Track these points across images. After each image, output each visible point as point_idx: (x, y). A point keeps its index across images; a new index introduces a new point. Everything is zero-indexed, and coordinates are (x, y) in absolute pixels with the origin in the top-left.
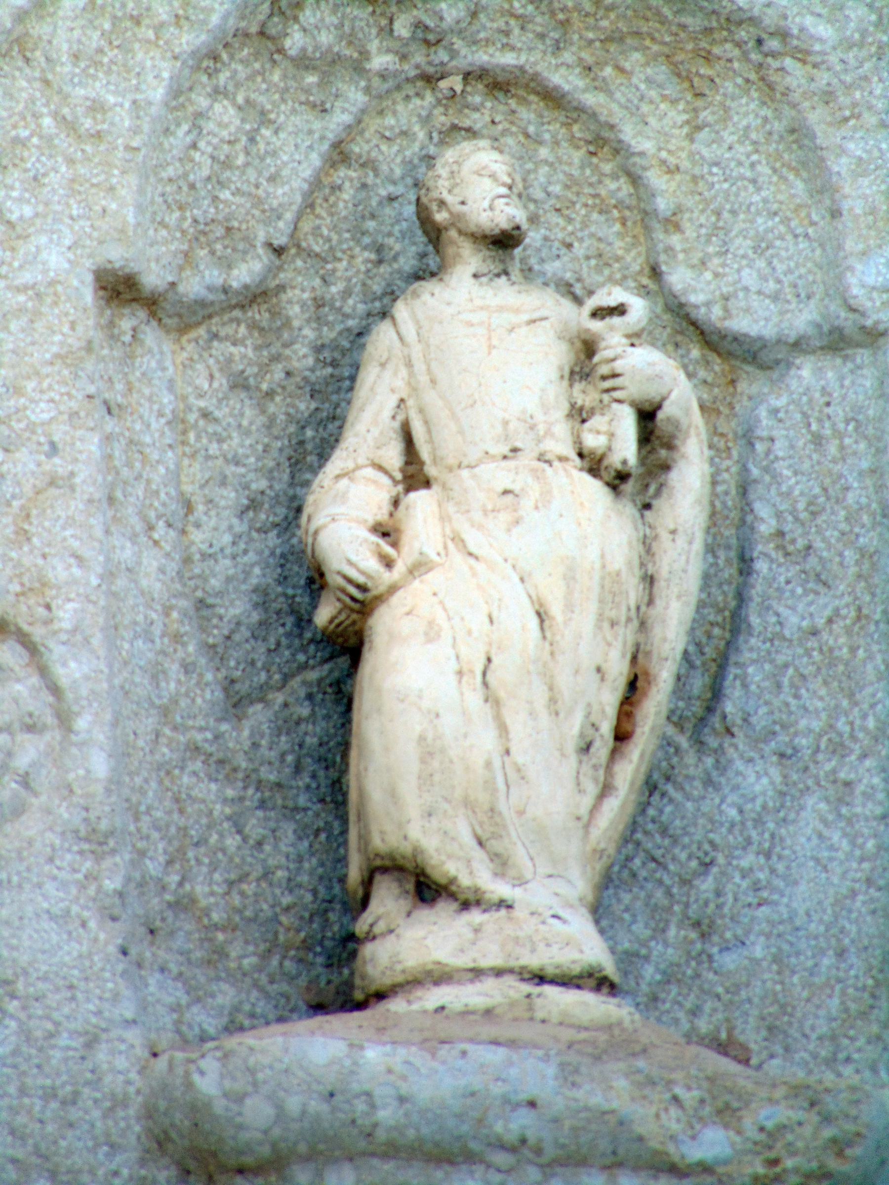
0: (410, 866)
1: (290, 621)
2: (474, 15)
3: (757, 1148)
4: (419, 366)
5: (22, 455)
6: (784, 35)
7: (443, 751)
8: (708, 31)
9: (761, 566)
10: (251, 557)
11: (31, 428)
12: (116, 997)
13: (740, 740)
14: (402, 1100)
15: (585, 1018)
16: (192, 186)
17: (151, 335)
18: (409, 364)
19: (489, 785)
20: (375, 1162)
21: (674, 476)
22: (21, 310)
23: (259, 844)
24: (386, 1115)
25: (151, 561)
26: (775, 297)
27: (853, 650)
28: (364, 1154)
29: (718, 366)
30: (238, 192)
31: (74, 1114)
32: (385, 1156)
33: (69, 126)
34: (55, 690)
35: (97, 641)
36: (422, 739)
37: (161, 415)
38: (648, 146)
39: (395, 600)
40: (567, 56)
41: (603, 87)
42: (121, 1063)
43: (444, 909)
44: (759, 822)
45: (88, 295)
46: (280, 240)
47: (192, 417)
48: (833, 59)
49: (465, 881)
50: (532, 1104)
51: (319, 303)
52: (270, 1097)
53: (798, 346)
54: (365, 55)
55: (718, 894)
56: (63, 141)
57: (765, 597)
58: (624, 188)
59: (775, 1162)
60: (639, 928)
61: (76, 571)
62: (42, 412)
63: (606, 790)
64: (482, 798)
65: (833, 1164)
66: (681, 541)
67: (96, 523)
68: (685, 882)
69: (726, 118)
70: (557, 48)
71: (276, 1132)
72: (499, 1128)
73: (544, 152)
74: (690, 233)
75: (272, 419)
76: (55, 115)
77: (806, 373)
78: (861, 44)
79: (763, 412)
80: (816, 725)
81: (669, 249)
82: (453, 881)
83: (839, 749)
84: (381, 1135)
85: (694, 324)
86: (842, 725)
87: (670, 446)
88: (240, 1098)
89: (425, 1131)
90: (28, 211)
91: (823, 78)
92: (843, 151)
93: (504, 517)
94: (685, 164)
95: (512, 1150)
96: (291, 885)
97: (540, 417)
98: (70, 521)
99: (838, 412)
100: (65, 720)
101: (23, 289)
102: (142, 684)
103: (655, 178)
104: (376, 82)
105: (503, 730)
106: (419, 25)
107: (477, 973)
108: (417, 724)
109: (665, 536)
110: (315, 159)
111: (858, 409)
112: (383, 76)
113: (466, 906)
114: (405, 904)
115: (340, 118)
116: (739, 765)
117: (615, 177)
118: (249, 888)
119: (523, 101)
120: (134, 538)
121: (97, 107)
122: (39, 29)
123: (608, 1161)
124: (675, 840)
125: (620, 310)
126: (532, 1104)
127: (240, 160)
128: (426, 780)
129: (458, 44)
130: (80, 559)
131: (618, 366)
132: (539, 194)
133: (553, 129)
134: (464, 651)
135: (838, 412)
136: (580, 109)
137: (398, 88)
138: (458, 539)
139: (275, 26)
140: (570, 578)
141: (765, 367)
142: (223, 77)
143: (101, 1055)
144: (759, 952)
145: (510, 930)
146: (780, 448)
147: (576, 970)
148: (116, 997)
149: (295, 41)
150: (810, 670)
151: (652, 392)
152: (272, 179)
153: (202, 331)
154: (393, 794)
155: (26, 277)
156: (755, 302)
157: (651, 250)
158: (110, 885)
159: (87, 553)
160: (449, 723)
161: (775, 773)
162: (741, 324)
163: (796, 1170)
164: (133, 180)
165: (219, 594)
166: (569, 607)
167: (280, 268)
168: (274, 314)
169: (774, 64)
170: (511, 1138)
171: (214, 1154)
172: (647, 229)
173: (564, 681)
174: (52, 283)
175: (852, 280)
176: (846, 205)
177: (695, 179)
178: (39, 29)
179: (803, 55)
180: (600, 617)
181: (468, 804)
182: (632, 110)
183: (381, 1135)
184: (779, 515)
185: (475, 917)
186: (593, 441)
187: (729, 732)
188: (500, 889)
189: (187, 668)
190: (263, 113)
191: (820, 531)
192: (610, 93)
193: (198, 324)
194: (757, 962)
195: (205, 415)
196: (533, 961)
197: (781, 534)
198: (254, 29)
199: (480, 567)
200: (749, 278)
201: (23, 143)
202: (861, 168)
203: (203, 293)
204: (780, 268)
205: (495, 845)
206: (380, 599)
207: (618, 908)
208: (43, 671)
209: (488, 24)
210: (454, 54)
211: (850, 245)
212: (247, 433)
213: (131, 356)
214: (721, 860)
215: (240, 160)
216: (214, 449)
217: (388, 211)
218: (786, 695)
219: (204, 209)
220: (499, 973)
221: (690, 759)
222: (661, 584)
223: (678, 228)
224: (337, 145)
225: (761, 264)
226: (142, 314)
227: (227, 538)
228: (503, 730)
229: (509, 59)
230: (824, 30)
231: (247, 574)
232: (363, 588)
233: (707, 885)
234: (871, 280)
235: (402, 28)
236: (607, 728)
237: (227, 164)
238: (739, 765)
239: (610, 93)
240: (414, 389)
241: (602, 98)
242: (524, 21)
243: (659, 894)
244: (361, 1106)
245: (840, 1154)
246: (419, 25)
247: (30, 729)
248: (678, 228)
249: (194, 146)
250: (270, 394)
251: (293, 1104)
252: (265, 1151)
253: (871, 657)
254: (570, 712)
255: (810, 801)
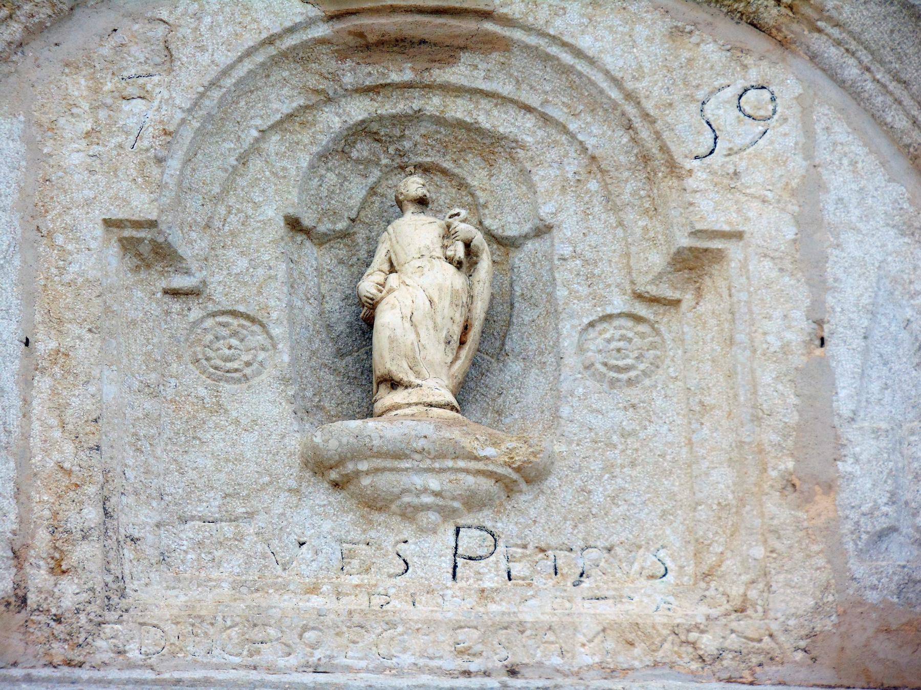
0: (388, 377)
1: (360, 332)
2: (415, 145)
3: (505, 454)
4: (394, 239)
5: (260, 270)
6: (516, 142)
7: (397, 340)
8: (492, 144)
9: (517, 305)
10: (346, 313)
11: (263, 262)
12: (291, 424)
13: (511, 357)
14: (381, 437)
15: (446, 416)
16: (321, 198)
17: (308, 244)
18: (391, 240)
19: (413, 350)
20: (374, 459)
21: (479, 266)
22: (259, 228)
23: (349, 394)
24: (376, 443)
25: (308, 309)
26: (518, 223)
27: (545, 323)
28: (370, 456)
29: (502, 249)
30: (337, 201)
31: (277, 458)
32: (377, 457)
33: (275, 174)
34: (271, 338)
35: (285, 322)
36: (389, 337)
37: (312, 267)
38: (476, 183)
39: (383, 302)
40: (448, 157)
41: (460, 166)
42: (293, 443)
43: (400, 389)
44: (517, 379)
45: (282, 224)
46: (354, 217)
47: (325, 271)
48: (533, 147)
49: (405, 379)
50: (425, 437)
51: (368, 238)
52: (337, 439)
53: (526, 237)
54: (379, 159)
55: (504, 402)
56: (272, 179)
57: (518, 314)
58: (469, 199)
59: (512, 458)
60: (478, 415)
61: (278, 303)
62: (266, 257)
63: (456, 358)
64: (410, 354)
65: (532, 459)
66: (481, 284)
67: (285, 289)
68: (494, 400)
69: (500, 172)
70: (444, 155)
71: (339, 450)
72: (415, 445)
73: (443, 190)
74: (491, 208)
75: (353, 273)
76: (270, 171)
77: (529, 245)
78: (542, 143)
79: (516, 260)
80: (534, 348)
81: (484, 214)
82: (401, 380)
83: (542, 353)
84: (375, 450)
85: (493, 236)
86: (542, 346)
87: (477, 256)
88: (327, 441)
89: (390, 447)
90: (261, 199)
91: (530, 154)
92: (537, 174)
93: (418, 274)
94: (488, 188)
95: (420, 453)
96: (359, 406)
97: (431, 246)
98: (276, 288)
99: (539, 255)
100: (274, 347)
101: (260, 221)
102: (305, 342)
103: (479, 193)
104: (384, 168)
105: (418, 334)
106: (397, 149)
107: (409, 405)
108: (388, 333)
109: (476, 283)
110: (364, 192)
111: (546, 252)
112: (386, 166)
113: (406, 387)
114: (387, 391)
115: (372, 180)
116: (511, 364)
117: (466, 196)
118: (345, 406)
119: (435, 175)
120: (302, 300)
121: (284, 169)
122: (263, 146)
123: (453, 456)
124: (490, 388)
125: (458, 214)
126: (425, 437)
127: (338, 191)
128: (391, 349)
129: (411, 155)
130: (279, 299)
131: (457, 229)
132: (442, 203)
133: (445, 183)
134: (403, 311)
135: (539, 255)
136: (453, 175)
137: (392, 170)
138: (404, 282)
139: (347, 149)
140: (440, 290)
141: (517, 247)
142: (330, 164)
143: (287, 440)
144: (517, 416)
145: (420, 392)
146: (522, 269)
147: (443, 403)
148: (291, 424)
149: (355, 154)
150: (532, 332)
151: (469, 236)
152: (349, 198)
153: (327, 245)
154: (382, 356)
155: (261, 218)
156: (512, 226)
157: (479, 216)
158: (290, 393)
159: (281, 297)
160: (399, 332)
161: (522, 364)
162: (508, 233)
163: (520, 460)
164: (296, 190)
165: (335, 323)
166: (440, 298)
167: (354, 227)
168: (353, 241)
169: (514, 151)
170: (419, 448)
171: (322, 463)
172: (477, 210)
173: (439, 320)
174: (270, 220)
175: (541, 211)
176: (538, 190)
177: (492, 192)
178: (263, 146)
179: (523, 147)
180: (451, 303)
181: (406, 356)
182: (470, 173)
183: (375, 450)
184: (522, 289)
185: (410, 390)
186: (449, 253)
187: (507, 355)
188: (419, 382)
189: (322, 341)
190: (345, 177)
191: (535, 291)
192: (462, 168)
193: (326, 243)
194: (516, 419)
195: (330, 271)
196: (428, 400)
197: (523, 294)
198: (340, 150)
199: (410, 288)
200: (510, 219)
201: (260, 179)
202: (543, 178)
203: (325, 231)
204: (520, 214)
205: (416, 368)
206: (378, 302)
207: (471, 410)
208: (268, 333)
209: (420, 148)
210: (410, 159)
211: (539, 201)
212: (344, 277)
213: (301, 248)
214: (505, 392)
215: (338, 191)
216: (332, 281)
217: (391, 210)
218: (525, 341)
219: (326, 206)
220: (416, 404)
221: (495, 365)
222: (475, 298)
223: (487, 207)
224: (372, 188)
225: (514, 214)
226: (305, 237)
227: (337, 307)
228: (418, 334)
229: (428, 159)
230: (529, 139)
231: (345, 318)
232: (372, 299)
233: (500, 400)
234: (547, 211)
235: (391, 150)
236: (456, 338)
237: (333, 192)
238: (511, 364)
239: (462, 168)
240: (392, 246)
241: (460, 170)
242: (433, 147)
243: (485, 405)
244: (367, 440)
245: (535, 456)
246: (397, 149)
247: (263, 349)
248: (487, 207)
249: (321, 185)
250: (352, 265)
251: (344, 440)
252: (337, 457)
253: (551, 324)
254: (442, 330)
255: (533, 370)
